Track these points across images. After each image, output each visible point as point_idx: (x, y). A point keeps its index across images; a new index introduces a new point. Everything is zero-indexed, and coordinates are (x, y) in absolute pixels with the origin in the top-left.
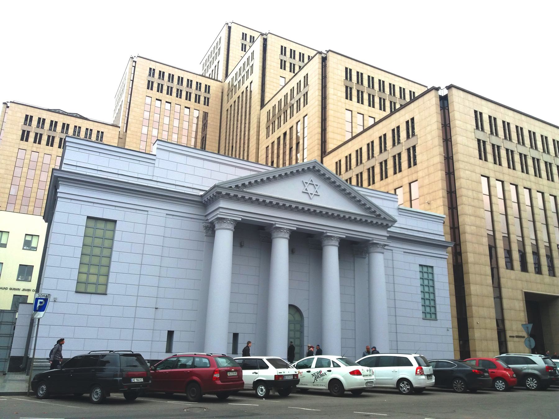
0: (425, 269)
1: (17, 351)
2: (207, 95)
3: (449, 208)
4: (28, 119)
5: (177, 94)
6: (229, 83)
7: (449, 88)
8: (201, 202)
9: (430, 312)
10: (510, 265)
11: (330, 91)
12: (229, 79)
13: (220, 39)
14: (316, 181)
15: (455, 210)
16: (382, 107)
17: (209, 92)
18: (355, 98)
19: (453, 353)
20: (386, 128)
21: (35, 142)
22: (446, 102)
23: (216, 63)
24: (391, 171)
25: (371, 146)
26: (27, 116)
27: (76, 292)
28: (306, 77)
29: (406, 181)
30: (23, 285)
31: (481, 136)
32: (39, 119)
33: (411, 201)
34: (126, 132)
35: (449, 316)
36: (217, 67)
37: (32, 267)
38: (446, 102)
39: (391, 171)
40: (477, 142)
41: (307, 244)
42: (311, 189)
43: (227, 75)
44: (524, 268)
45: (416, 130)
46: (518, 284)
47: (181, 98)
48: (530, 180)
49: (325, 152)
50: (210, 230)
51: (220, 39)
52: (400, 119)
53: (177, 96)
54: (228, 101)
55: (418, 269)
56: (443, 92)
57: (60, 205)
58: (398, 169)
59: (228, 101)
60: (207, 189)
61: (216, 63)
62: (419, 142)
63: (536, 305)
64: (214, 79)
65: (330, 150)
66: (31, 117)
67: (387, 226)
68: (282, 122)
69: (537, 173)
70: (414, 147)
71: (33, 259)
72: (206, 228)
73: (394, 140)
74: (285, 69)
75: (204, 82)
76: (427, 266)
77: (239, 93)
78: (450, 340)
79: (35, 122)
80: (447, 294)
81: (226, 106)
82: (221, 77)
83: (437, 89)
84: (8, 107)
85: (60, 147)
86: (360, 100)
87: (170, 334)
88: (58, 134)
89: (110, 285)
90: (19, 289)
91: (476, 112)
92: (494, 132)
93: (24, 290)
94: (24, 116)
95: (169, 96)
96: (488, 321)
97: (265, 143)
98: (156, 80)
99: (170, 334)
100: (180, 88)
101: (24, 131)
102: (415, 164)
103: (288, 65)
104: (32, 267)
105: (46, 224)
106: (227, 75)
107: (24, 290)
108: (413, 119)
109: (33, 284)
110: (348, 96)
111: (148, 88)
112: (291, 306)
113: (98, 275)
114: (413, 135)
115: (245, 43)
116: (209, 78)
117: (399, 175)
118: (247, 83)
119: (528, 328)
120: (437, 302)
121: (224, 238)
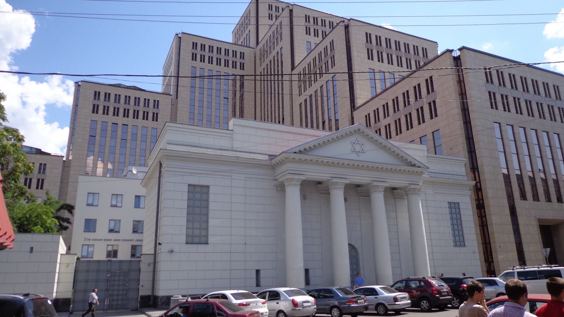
1: (144, 291)
2: (242, 61)
3: (469, 152)
4: (97, 95)
5: (217, 62)
6: (261, 49)
7: (460, 49)
8: (271, 166)
9: (459, 240)
10: (523, 196)
11: (354, 54)
12: (260, 45)
13: (249, 11)
14: (361, 140)
15: (473, 154)
17: (243, 58)
18: (375, 58)
19: (79, 180)
20: (408, 85)
22: (459, 61)
23: (247, 32)
25: (396, 101)
26: (96, 92)
27: (187, 243)
28: (332, 43)
29: (429, 131)
31: (491, 88)
32: (106, 93)
33: (435, 147)
34: (177, 98)
35: (476, 244)
36: (249, 35)
38: (459, 61)
40: (488, 94)
41: (358, 193)
43: (257, 43)
44: (536, 197)
45: (435, 87)
46: (531, 213)
47: (220, 65)
48: (536, 122)
49: (354, 106)
50: (281, 188)
51: (249, 11)
52: (421, 78)
53: (217, 64)
54: (261, 65)
56: (456, 54)
59: (261, 65)
61: (247, 32)
62: (438, 96)
63: (548, 232)
64: (247, 46)
66: (99, 93)
70: (434, 102)
72: (276, 186)
74: (310, 34)
75: (239, 49)
77: (271, 57)
78: (478, 263)
80: (472, 224)
82: (253, 43)
83: (451, 51)
84: (79, 86)
86: (380, 59)
87: (258, 272)
89: (209, 237)
90: (111, 240)
92: (502, 83)
94: (94, 92)
95: (210, 65)
97: (298, 100)
98: (199, 52)
99: (258, 272)
100: (219, 56)
101: (94, 105)
102: (436, 116)
106: (257, 43)
107: (115, 240)
108: (431, 78)
110: (370, 56)
111: (193, 59)
112: (350, 245)
113: (200, 229)
114: (433, 90)
115: (271, 12)
116: (242, 45)
117: (423, 125)
118: (277, 49)
119: (546, 251)
120: (464, 232)
121: (293, 194)
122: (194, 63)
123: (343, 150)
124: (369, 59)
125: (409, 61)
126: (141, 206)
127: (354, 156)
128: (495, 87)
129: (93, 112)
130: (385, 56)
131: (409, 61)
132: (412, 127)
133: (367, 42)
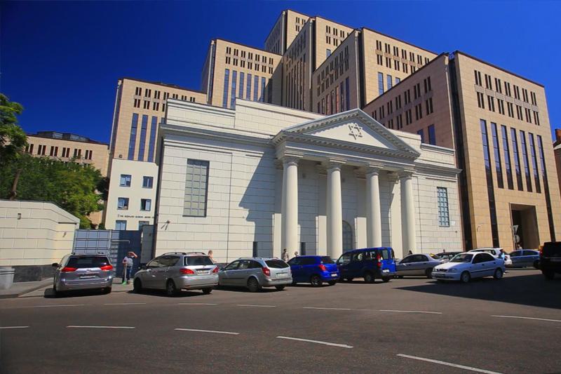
0: (441, 190)
9: (445, 221)
10: (501, 185)
16: (405, 70)
21: (145, 108)
24: (414, 117)
27: (184, 216)
30: (144, 214)
37: (139, 222)
39: (414, 117)
42: (355, 132)
44: (511, 187)
46: (506, 198)
55: (436, 190)
57: (167, 151)
58: (419, 116)
60: (275, 134)
65: (367, 103)
67: (414, 159)
68: (344, 69)
69: (520, 117)
70: (431, 99)
71: (150, 194)
73: (397, 106)
76: (442, 188)
79: (143, 93)
81: (286, 73)
85: (163, 111)
88: (161, 101)
91: (475, 71)
93: (146, 217)
95: (235, 66)
96: (486, 225)
102: (432, 112)
103: (332, 40)
104: (139, 222)
105: (158, 167)
107: (146, 217)
108: (429, 78)
109: (152, 213)
110: (379, 61)
117: (420, 120)
119: (515, 228)
122: (228, 66)
123: (342, 133)
124: (378, 63)
125: (405, 66)
126: (146, 209)
127: (351, 139)
128: (483, 89)
129: (135, 106)
130: (393, 62)
131: (405, 66)
132: (411, 122)
133: (378, 48)
